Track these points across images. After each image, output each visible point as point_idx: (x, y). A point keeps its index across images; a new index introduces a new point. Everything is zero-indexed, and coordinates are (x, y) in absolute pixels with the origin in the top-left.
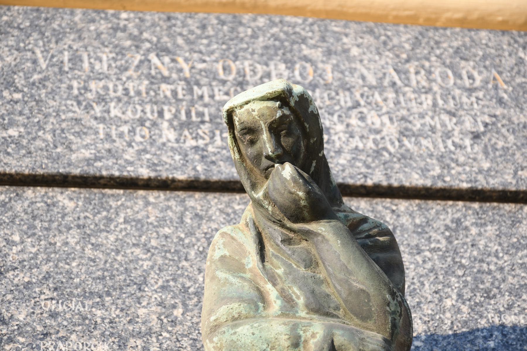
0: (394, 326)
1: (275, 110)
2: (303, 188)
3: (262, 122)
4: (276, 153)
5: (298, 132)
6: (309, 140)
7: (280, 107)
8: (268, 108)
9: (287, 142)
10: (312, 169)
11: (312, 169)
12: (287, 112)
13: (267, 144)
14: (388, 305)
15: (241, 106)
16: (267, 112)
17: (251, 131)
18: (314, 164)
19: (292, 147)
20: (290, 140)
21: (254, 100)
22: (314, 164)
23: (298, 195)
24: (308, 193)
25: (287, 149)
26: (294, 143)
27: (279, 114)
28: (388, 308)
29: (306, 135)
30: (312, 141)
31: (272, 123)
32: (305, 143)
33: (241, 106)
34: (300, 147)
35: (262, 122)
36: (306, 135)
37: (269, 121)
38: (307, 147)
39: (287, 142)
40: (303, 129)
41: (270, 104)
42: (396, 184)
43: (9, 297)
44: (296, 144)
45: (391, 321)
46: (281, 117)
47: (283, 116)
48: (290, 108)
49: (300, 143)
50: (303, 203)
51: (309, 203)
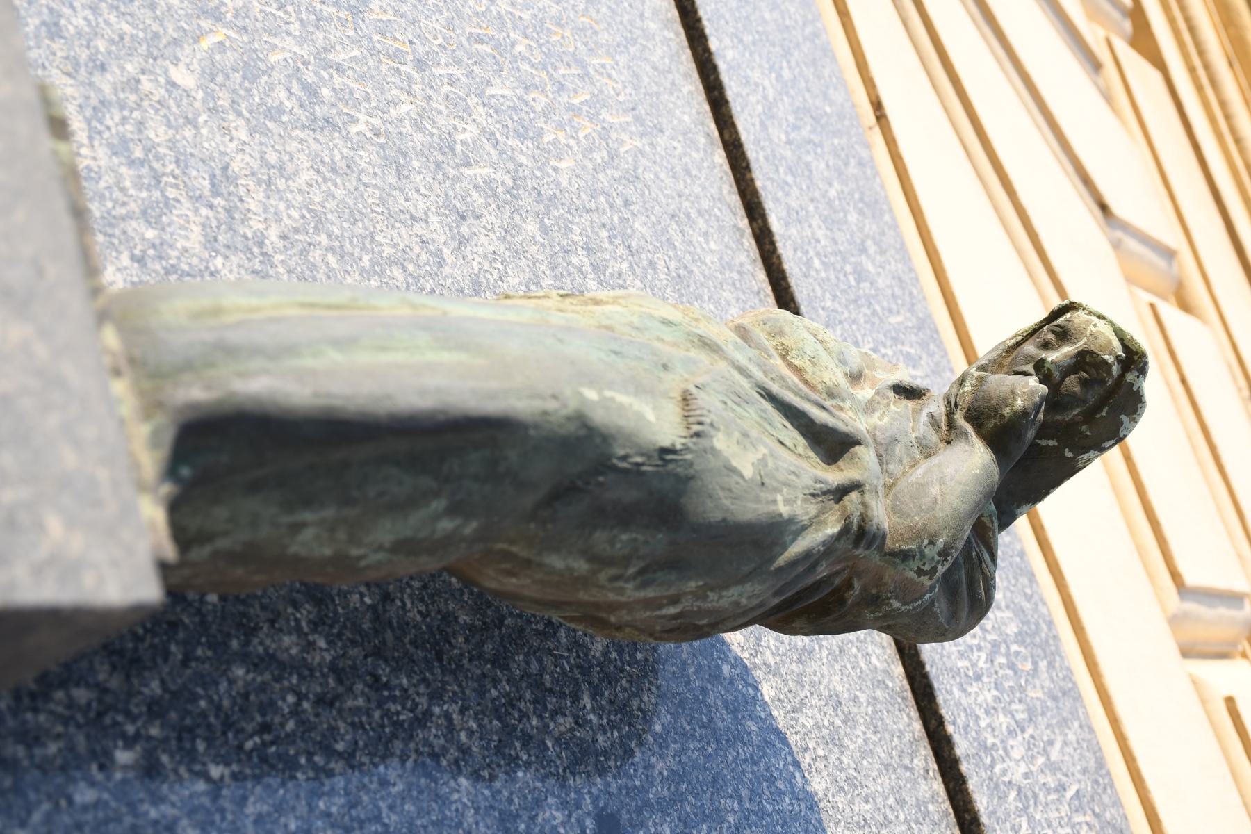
0: (906, 556)
1: (1111, 352)
2: (1028, 403)
3: (1085, 340)
4: (1053, 368)
5: (1092, 399)
6: (1084, 423)
7: (1117, 358)
8: (1110, 342)
9: (1072, 384)
10: (1043, 443)
11: (1043, 443)
12: (1116, 370)
13: (1061, 354)
14: (931, 543)
15: (1090, 313)
16: (1102, 341)
17: (1064, 335)
18: (1052, 443)
19: (1067, 395)
20: (1077, 389)
21: (1110, 322)
22: (1052, 443)
23: (1015, 400)
24: (1025, 413)
25: (1063, 388)
26: (1074, 395)
27: (1110, 358)
28: (926, 542)
29: (1090, 416)
30: (1084, 428)
31: (1091, 353)
32: (1077, 419)
33: (1090, 313)
34: (1072, 409)
35: (1085, 340)
36: (1090, 416)
37: (1092, 348)
38: (1072, 424)
39: (1072, 384)
40: (1098, 408)
41: (1116, 344)
42: (964, 767)
43: (653, 218)
44: (1074, 400)
45: (910, 550)
46: (1105, 361)
47: (1108, 366)
48: (1122, 376)
49: (1078, 406)
50: (1007, 411)
51: (1010, 420)
